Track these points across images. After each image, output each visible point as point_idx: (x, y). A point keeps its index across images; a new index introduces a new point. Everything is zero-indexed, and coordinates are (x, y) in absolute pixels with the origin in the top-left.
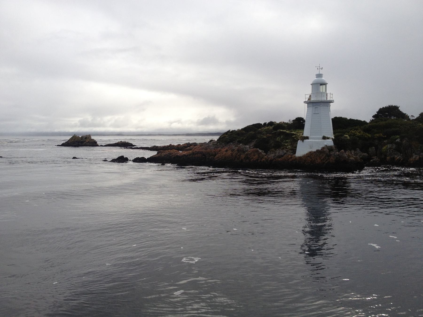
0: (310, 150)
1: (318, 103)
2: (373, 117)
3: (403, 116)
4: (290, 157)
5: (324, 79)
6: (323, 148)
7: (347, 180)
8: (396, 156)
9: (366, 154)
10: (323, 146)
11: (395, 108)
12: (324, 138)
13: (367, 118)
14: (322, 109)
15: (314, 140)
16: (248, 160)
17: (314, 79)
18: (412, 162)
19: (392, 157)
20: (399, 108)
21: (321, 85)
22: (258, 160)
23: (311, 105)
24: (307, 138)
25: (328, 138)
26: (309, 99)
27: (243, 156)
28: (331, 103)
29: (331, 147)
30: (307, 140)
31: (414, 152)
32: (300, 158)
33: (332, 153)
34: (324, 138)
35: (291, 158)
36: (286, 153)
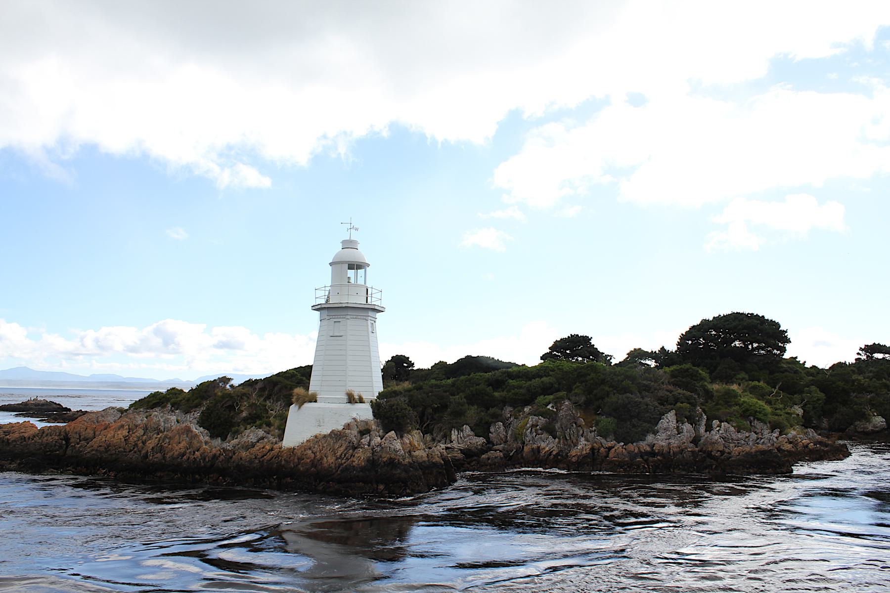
0: (317, 431)
1: (346, 310)
2: (542, 358)
3: (596, 354)
4: (268, 447)
5: (364, 253)
6: (348, 426)
7: (206, 553)
8: (543, 445)
9: (481, 440)
10: (348, 420)
11: (586, 340)
12: (351, 399)
13: (532, 360)
14: (350, 325)
15: (328, 405)
16: (159, 455)
17: (334, 250)
18: (574, 459)
19: (535, 446)
20: (593, 342)
21: (351, 267)
22: (183, 455)
23: (325, 312)
24: (313, 399)
25: (361, 401)
26: (327, 301)
27: (151, 444)
28: (378, 315)
29: (366, 423)
30: (313, 404)
31: (582, 436)
32: (292, 450)
33: (365, 440)
34: (351, 399)
35: (272, 449)
36: (263, 438)
